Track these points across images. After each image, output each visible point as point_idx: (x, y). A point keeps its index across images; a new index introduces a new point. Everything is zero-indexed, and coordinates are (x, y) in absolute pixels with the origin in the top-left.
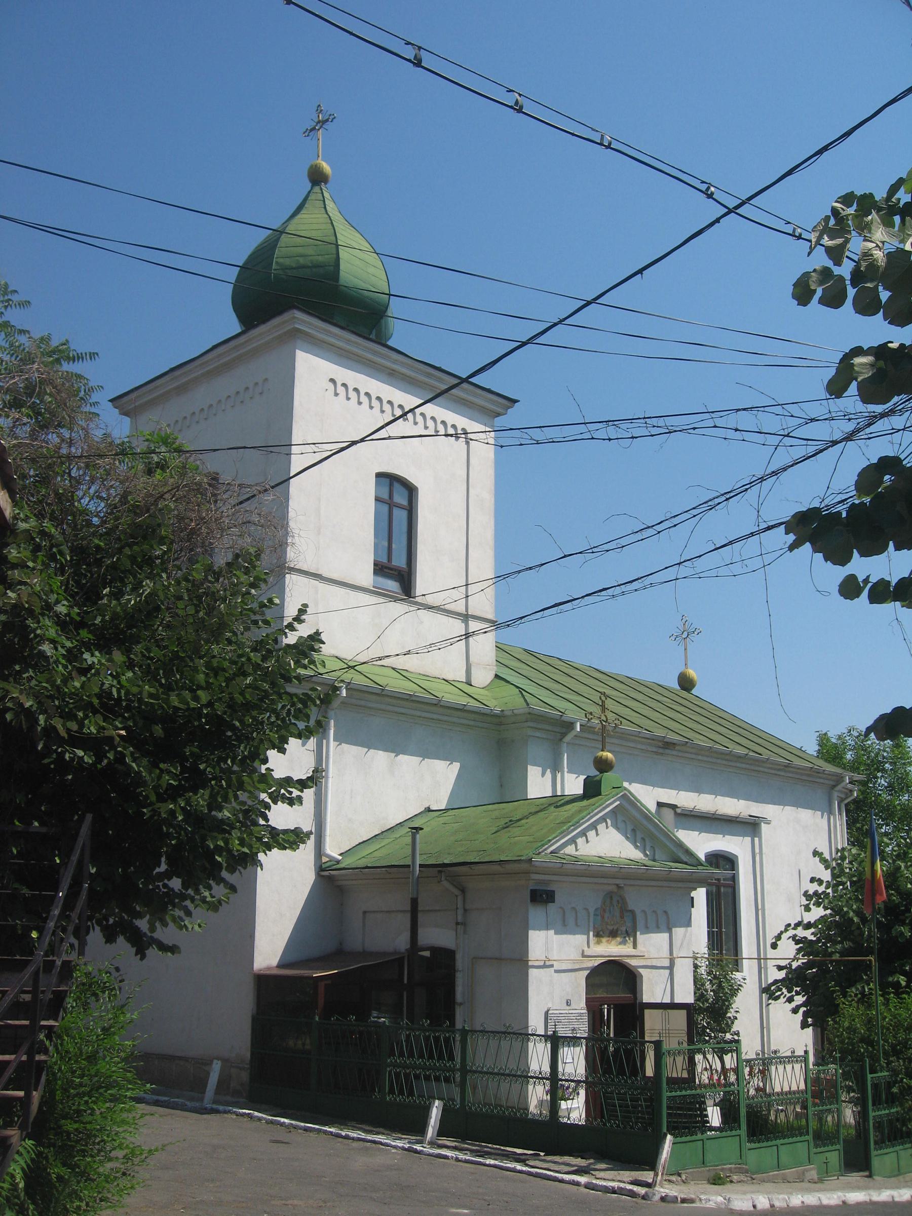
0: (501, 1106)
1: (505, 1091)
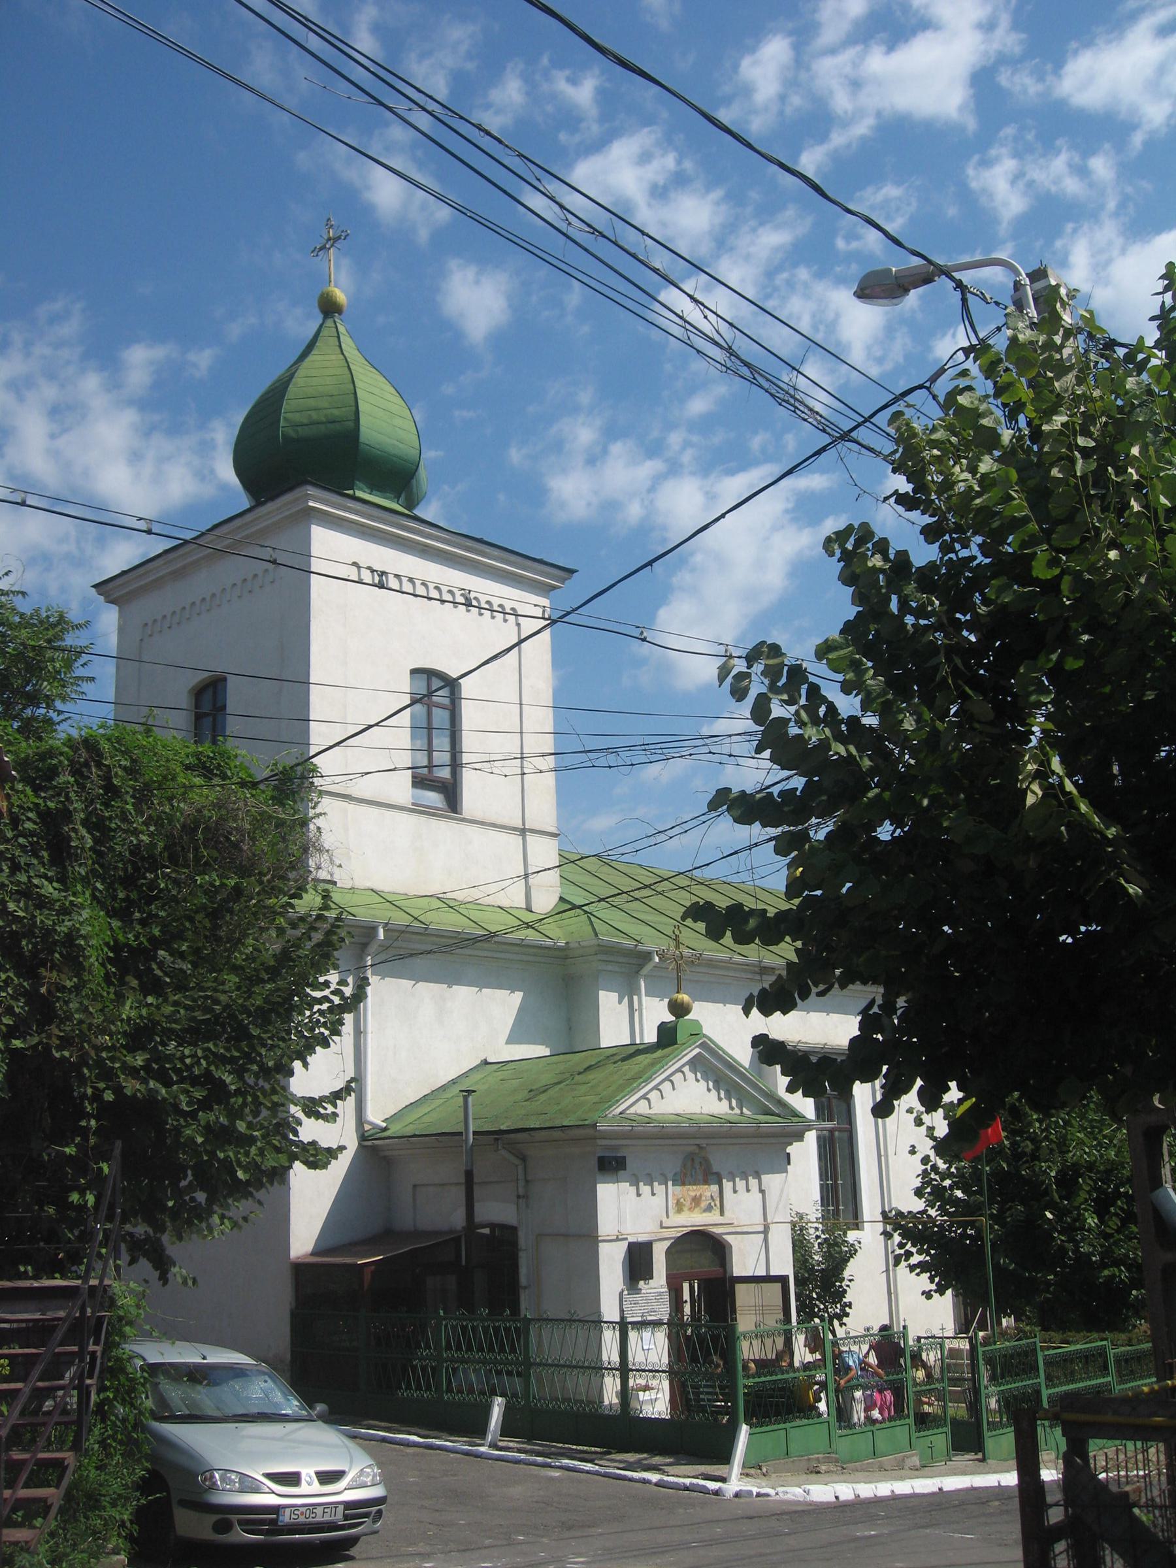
1: (575, 1385)
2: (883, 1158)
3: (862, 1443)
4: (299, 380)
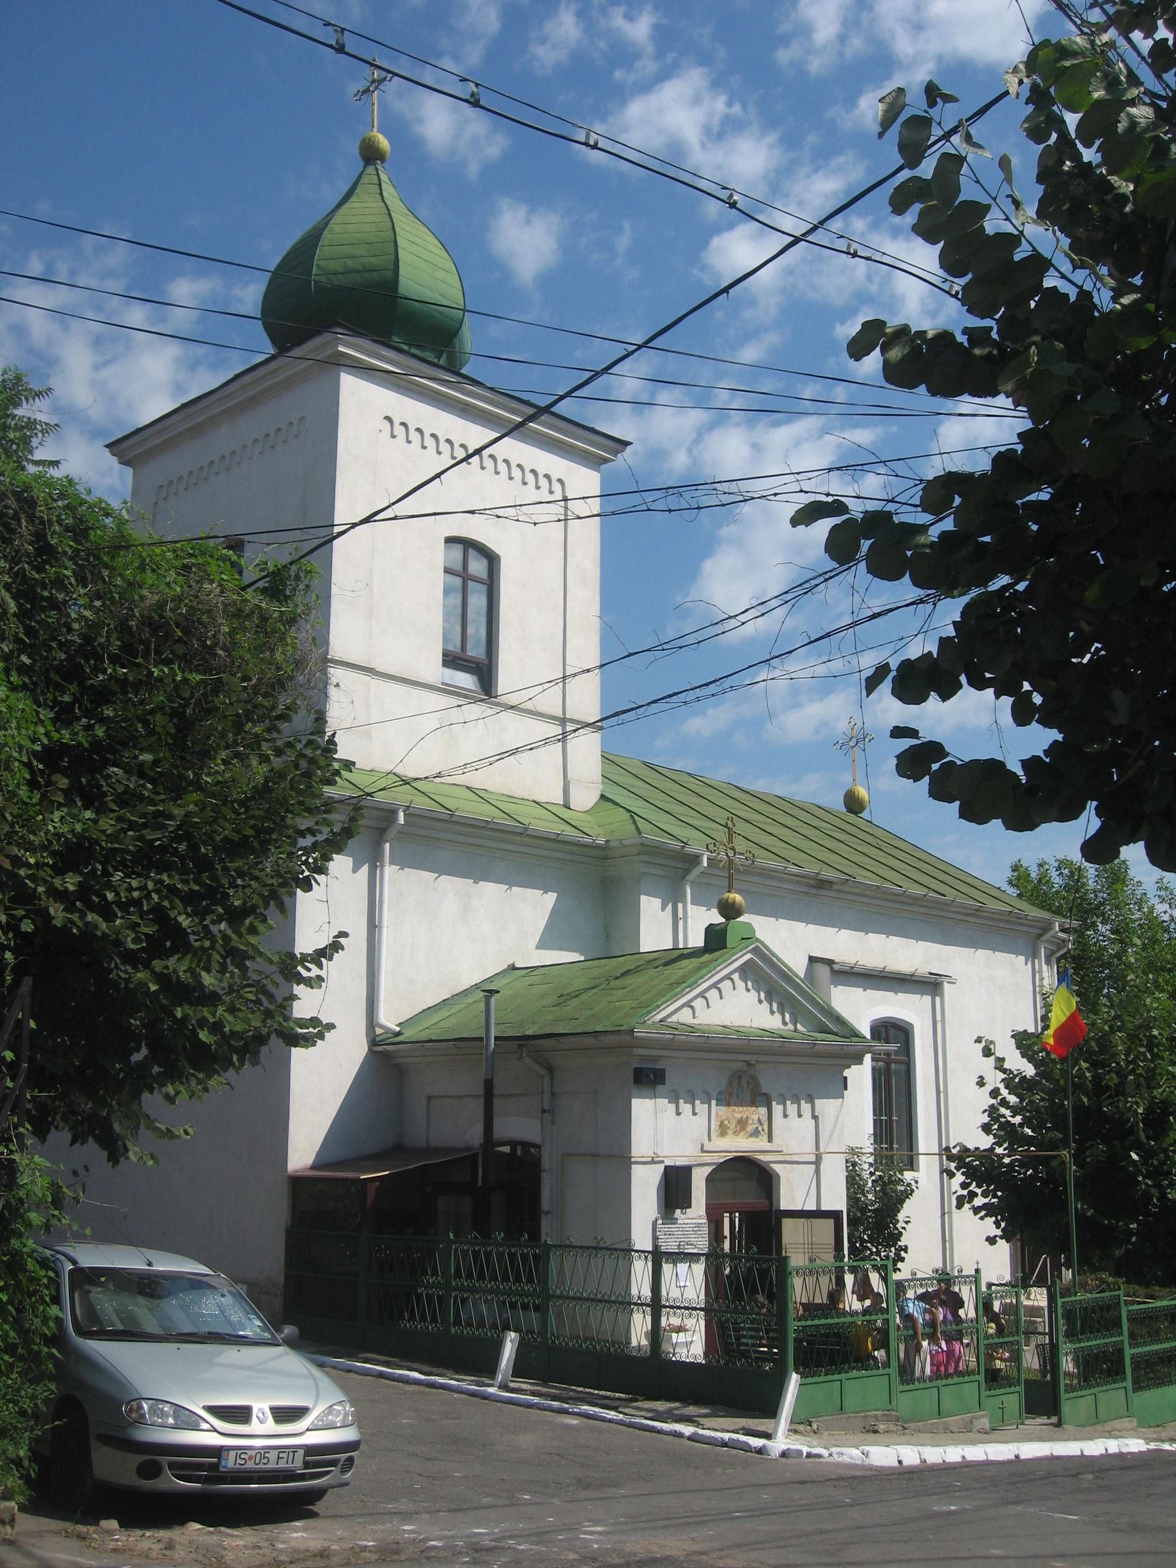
0: (606, 1341)
1: (599, 1322)
2: (942, 1094)
3: (924, 1399)
4: (336, 225)
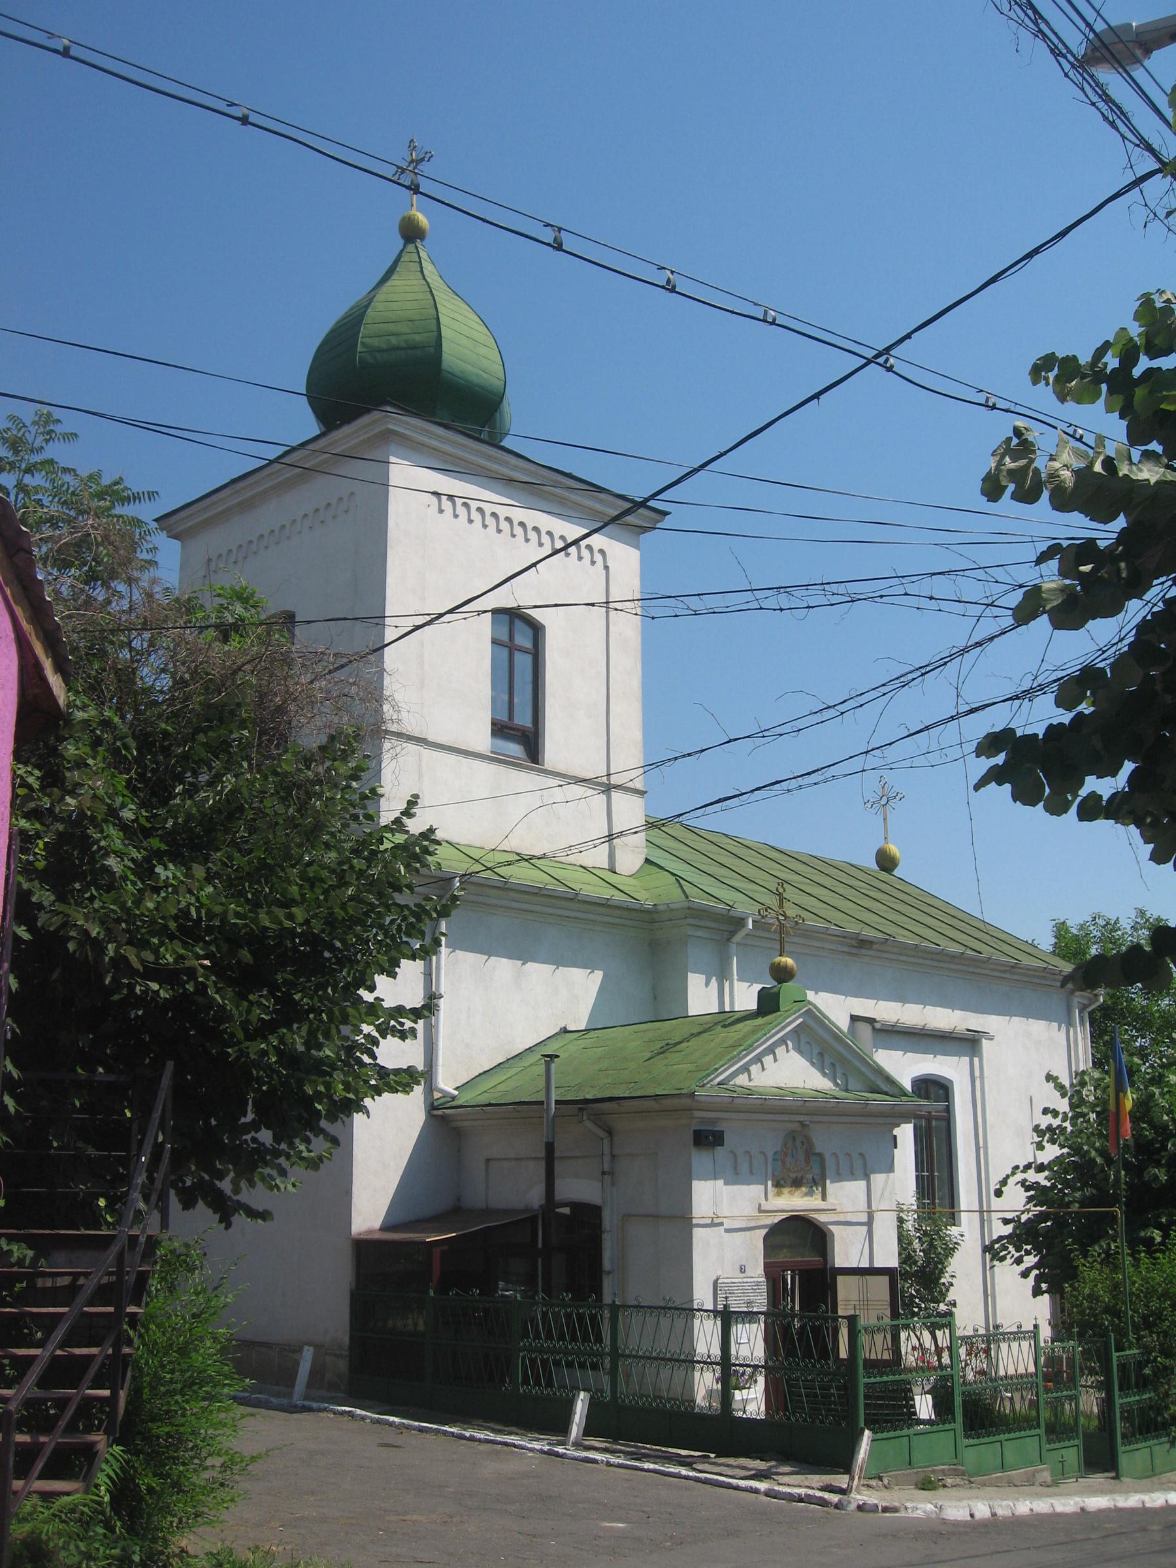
0: (661, 1398)
1: (665, 1380)
